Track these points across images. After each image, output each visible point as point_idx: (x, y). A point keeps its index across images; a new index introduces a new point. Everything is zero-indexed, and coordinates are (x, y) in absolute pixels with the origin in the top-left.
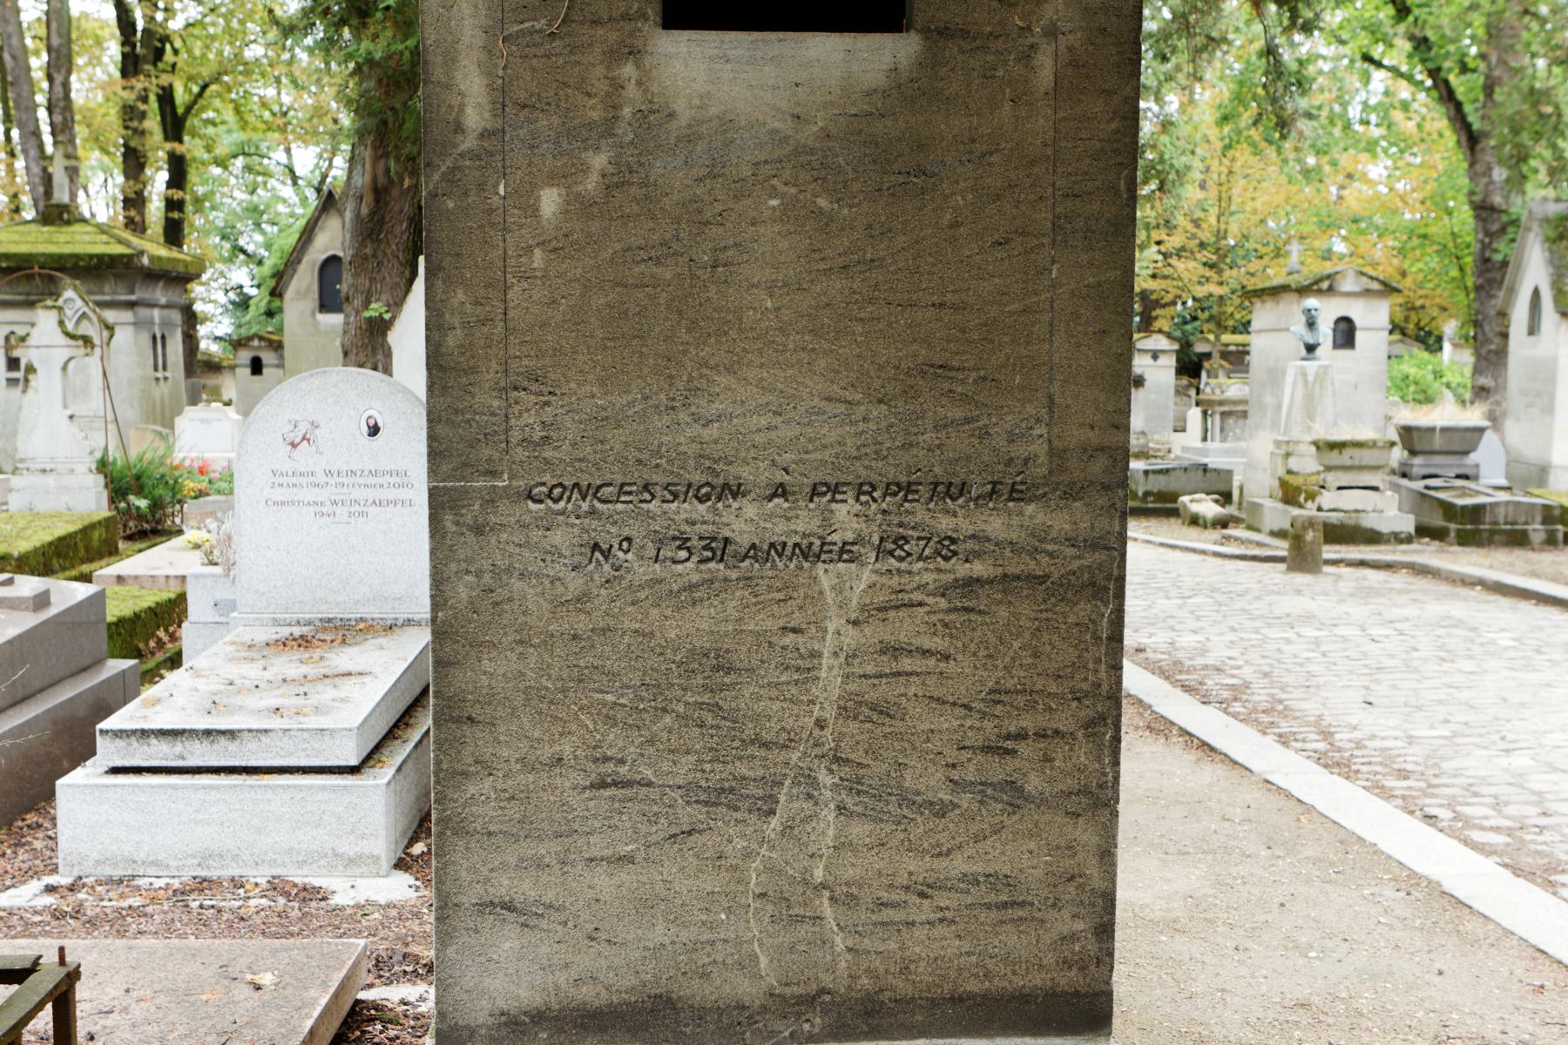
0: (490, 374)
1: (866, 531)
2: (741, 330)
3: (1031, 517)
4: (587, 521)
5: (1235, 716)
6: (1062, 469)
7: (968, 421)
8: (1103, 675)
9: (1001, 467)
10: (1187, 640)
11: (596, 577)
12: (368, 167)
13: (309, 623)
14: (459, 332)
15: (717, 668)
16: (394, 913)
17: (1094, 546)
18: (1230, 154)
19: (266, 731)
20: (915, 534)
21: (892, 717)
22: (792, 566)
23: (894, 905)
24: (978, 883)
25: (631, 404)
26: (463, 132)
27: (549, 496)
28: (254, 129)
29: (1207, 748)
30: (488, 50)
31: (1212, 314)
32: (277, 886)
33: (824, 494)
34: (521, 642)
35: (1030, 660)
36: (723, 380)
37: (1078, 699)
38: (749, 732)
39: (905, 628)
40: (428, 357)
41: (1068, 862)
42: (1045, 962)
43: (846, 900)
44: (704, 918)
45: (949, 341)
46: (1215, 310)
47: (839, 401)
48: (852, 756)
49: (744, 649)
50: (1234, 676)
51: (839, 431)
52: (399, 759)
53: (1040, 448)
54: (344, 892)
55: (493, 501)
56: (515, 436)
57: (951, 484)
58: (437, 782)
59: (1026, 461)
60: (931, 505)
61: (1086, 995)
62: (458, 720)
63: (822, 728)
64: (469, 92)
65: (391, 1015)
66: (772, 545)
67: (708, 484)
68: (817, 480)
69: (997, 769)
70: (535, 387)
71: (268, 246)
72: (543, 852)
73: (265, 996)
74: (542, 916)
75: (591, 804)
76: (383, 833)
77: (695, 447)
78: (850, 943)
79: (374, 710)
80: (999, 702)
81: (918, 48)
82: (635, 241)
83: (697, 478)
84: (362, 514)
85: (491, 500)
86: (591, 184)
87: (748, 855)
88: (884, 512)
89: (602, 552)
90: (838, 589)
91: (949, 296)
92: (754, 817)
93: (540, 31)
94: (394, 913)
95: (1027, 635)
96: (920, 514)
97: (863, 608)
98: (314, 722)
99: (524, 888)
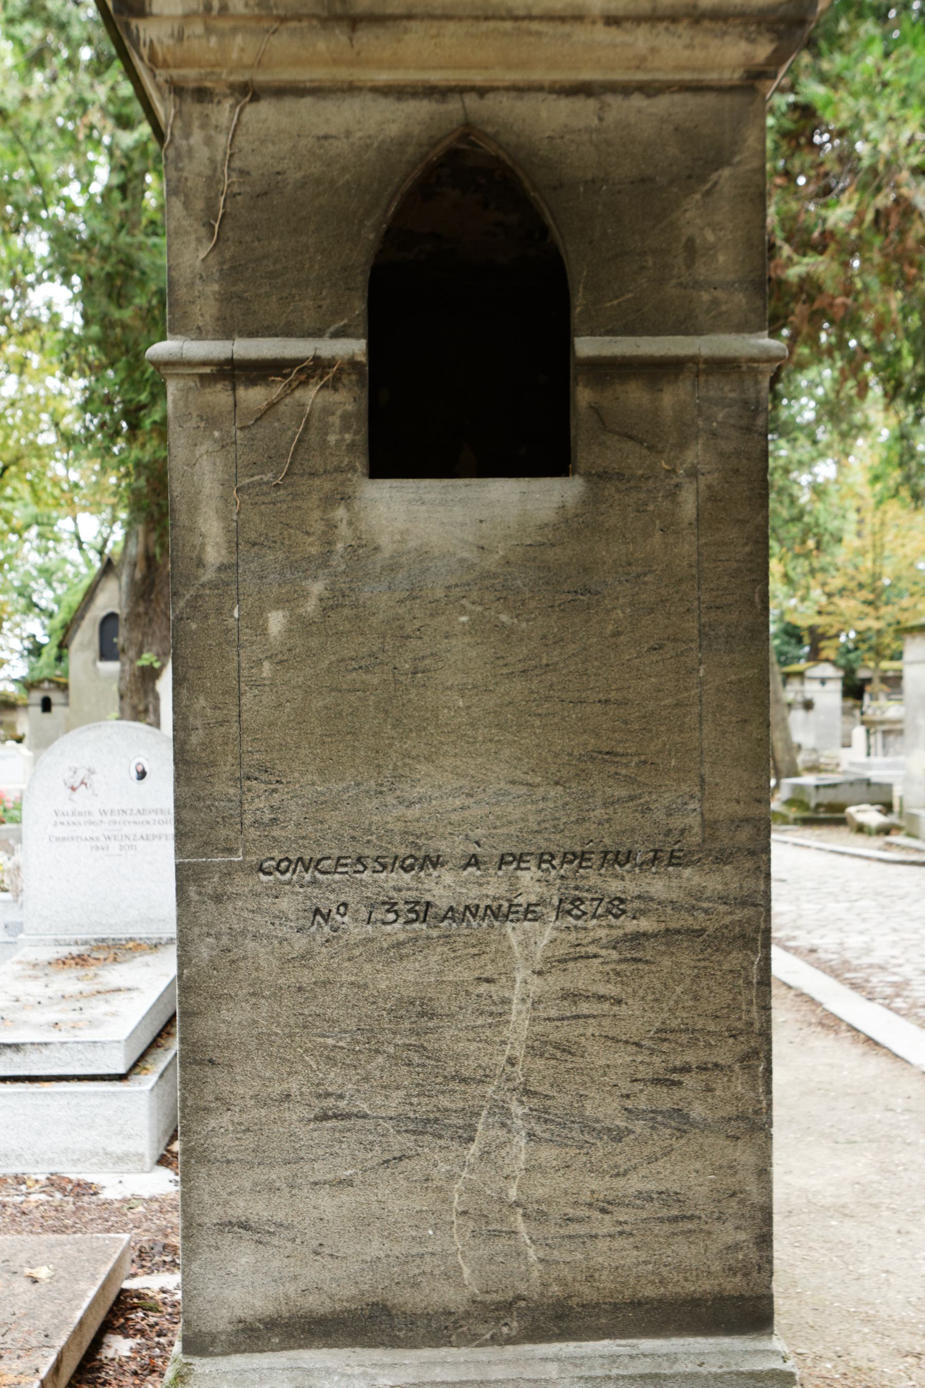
0: (227, 767)
1: (547, 895)
2: (437, 726)
3: (688, 879)
4: (309, 889)
5: (897, 1011)
6: (714, 838)
7: (632, 798)
8: (755, 1015)
9: (661, 837)
10: (855, 941)
11: (318, 937)
12: (141, 538)
13: (86, 943)
14: (201, 731)
15: (422, 1014)
16: (156, 1206)
17: (743, 903)
18: (882, 507)
19: (46, 1044)
20: (589, 896)
21: (573, 1055)
22: (485, 925)
23: (579, 1220)
24: (652, 1199)
25: (346, 790)
26: (204, 566)
27: (277, 869)
28: (47, 504)
29: (870, 1041)
30: (225, 499)
31: (872, 645)
32: (55, 1183)
33: (511, 863)
34: (254, 994)
35: (691, 1003)
36: (423, 768)
37: (734, 1036)
38: (450, 1070)
39: (582, 977)
40: (175, 754)
41: (730, 1180)
42: (713, 1269)
43: (538, 1217)
44: (414, 1233)
45: (614, 732)
46: (874, 641)
47: (521, 783)
48: (540, 1089)
49: (445, 997)
50: (895, 974)
51: (522, 809)
52: (162, 1066)
53: (694, 821)
54: (113, 1187)
55: (229, 874)
56: (248, 818)
57: (618, 852)
58: (183, 1117)
59: (683, 831)
60: (603, 871)
61: (750, 1298)
62: (200, 1063)
63: (513, 1065)
64: (209, 533)
65: (151, 1303)
66: (467, 908)
67: (411, 856)
68: (505, 851)
69: (666, 1099)
70: (264, 777)
71: (58, 601)
72: (274, 1177)
73: (41, 1288)
74: (273, 1233)
75: (315, 1134)
76: (147, 1134)
77: (400, 826)
78: (541, 1254)
79: (140, 1023)
80: (665, 1040)
81: (581, 489)
82: (346, 653)
83: (403, 851)
84: (131, 847)
85: (228, 873)
86: (310, 607)
87: (451, 1177)
88: (562, 877)
89: (322, 916)
90: (524, 944)
91: (613, 693)
92: (455, 1145)
93: (267, 483)
94: (156, 1206)
95: (688, 981)
96: (594, 879)
97: (547, 960)
98: (87, 1035)
99: (258, 1209)
